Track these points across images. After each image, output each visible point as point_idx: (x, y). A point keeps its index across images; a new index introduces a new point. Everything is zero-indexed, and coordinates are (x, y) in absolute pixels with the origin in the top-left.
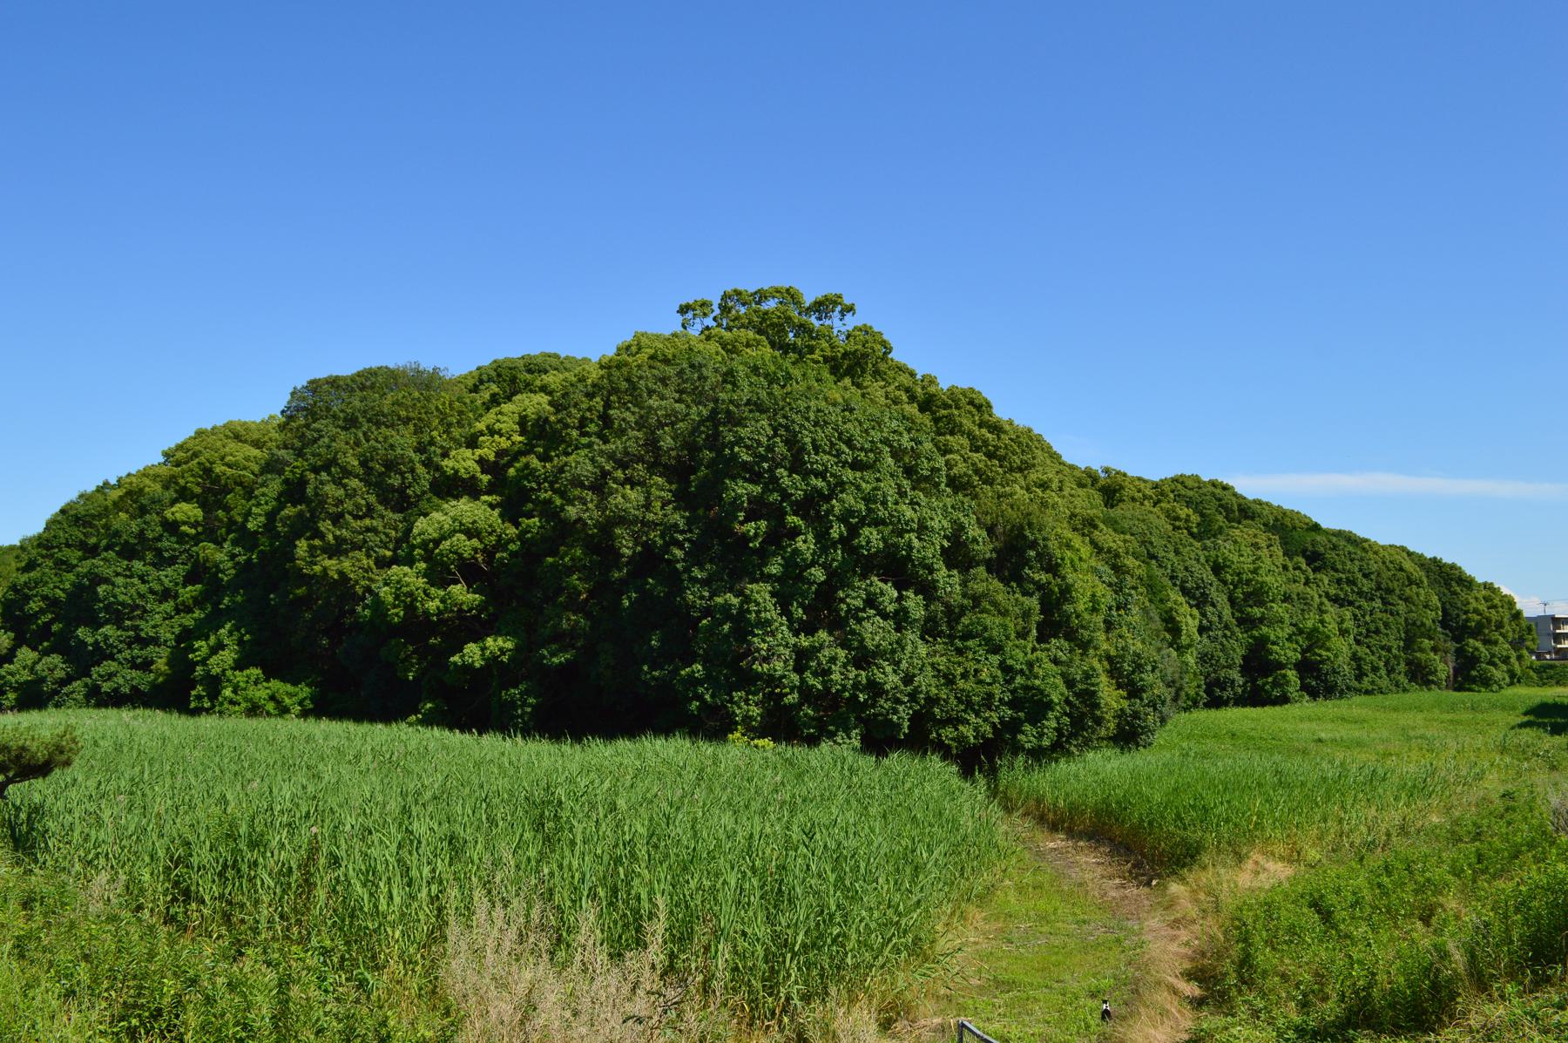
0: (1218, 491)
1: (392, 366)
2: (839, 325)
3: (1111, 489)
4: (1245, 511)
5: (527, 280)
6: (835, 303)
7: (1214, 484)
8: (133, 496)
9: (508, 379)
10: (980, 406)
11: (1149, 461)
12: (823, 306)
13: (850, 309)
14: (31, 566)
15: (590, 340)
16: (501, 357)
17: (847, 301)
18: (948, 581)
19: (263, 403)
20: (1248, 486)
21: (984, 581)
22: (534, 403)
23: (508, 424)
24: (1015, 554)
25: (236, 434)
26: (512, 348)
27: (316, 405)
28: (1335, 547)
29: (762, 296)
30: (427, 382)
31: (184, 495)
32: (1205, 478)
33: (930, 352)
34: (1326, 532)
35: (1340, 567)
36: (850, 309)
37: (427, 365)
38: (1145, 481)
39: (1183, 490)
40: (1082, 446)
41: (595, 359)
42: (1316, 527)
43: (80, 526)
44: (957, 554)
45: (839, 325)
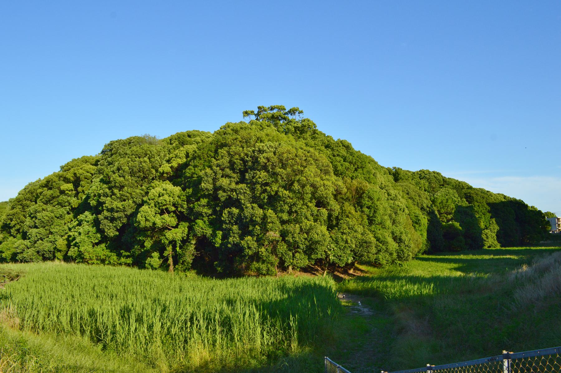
0: (436, 175)
1: (140, 135)
2: (297, 117)
3: (396, 175)
4: (445, 182)
5: (185, 103)
6: (296, 110)
7: (434, 172)
8: (48, 184)
9: (181, 140)
10: (348, 147)
11: (411, 165)
12: (292, 112)
13: (301, 112)
14: (13, 208)
15: (209, 125)
16: (179, 132)
17: (300, 110)
18: (335, 206)
19: (94, 150)
20: (446, 174)
21: (349, 208)
22: (191, 148)
23: (183, 154)
24: (359, 198)
25: (85, 160)
26: (183, 128)
27: (110, 150)
28: (477, 194)
29: (272, 109)
30: (151, 142)
31: (67, 180)
32: (431, 170)
33: (331, 128)
34: (474, 189)
35: (479, 201)
36: (301, 112)
37: (152, 135)
38: (410, 172)
39: (422, 175)
40: (386, 159)
41: (212, 132)
42: (471, 188)
43: (31, 195)
44: (337, 194)
45: (297, 117)
